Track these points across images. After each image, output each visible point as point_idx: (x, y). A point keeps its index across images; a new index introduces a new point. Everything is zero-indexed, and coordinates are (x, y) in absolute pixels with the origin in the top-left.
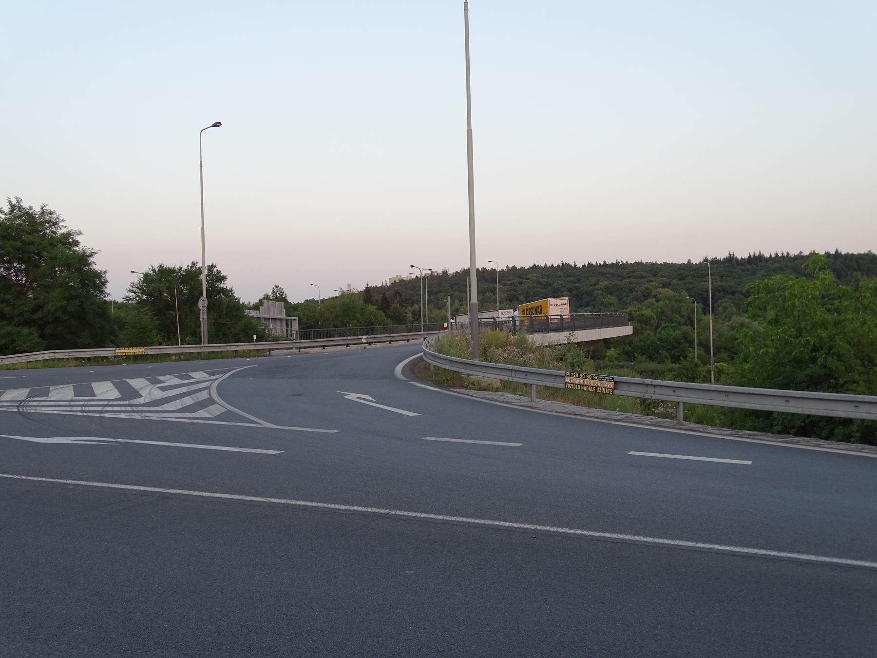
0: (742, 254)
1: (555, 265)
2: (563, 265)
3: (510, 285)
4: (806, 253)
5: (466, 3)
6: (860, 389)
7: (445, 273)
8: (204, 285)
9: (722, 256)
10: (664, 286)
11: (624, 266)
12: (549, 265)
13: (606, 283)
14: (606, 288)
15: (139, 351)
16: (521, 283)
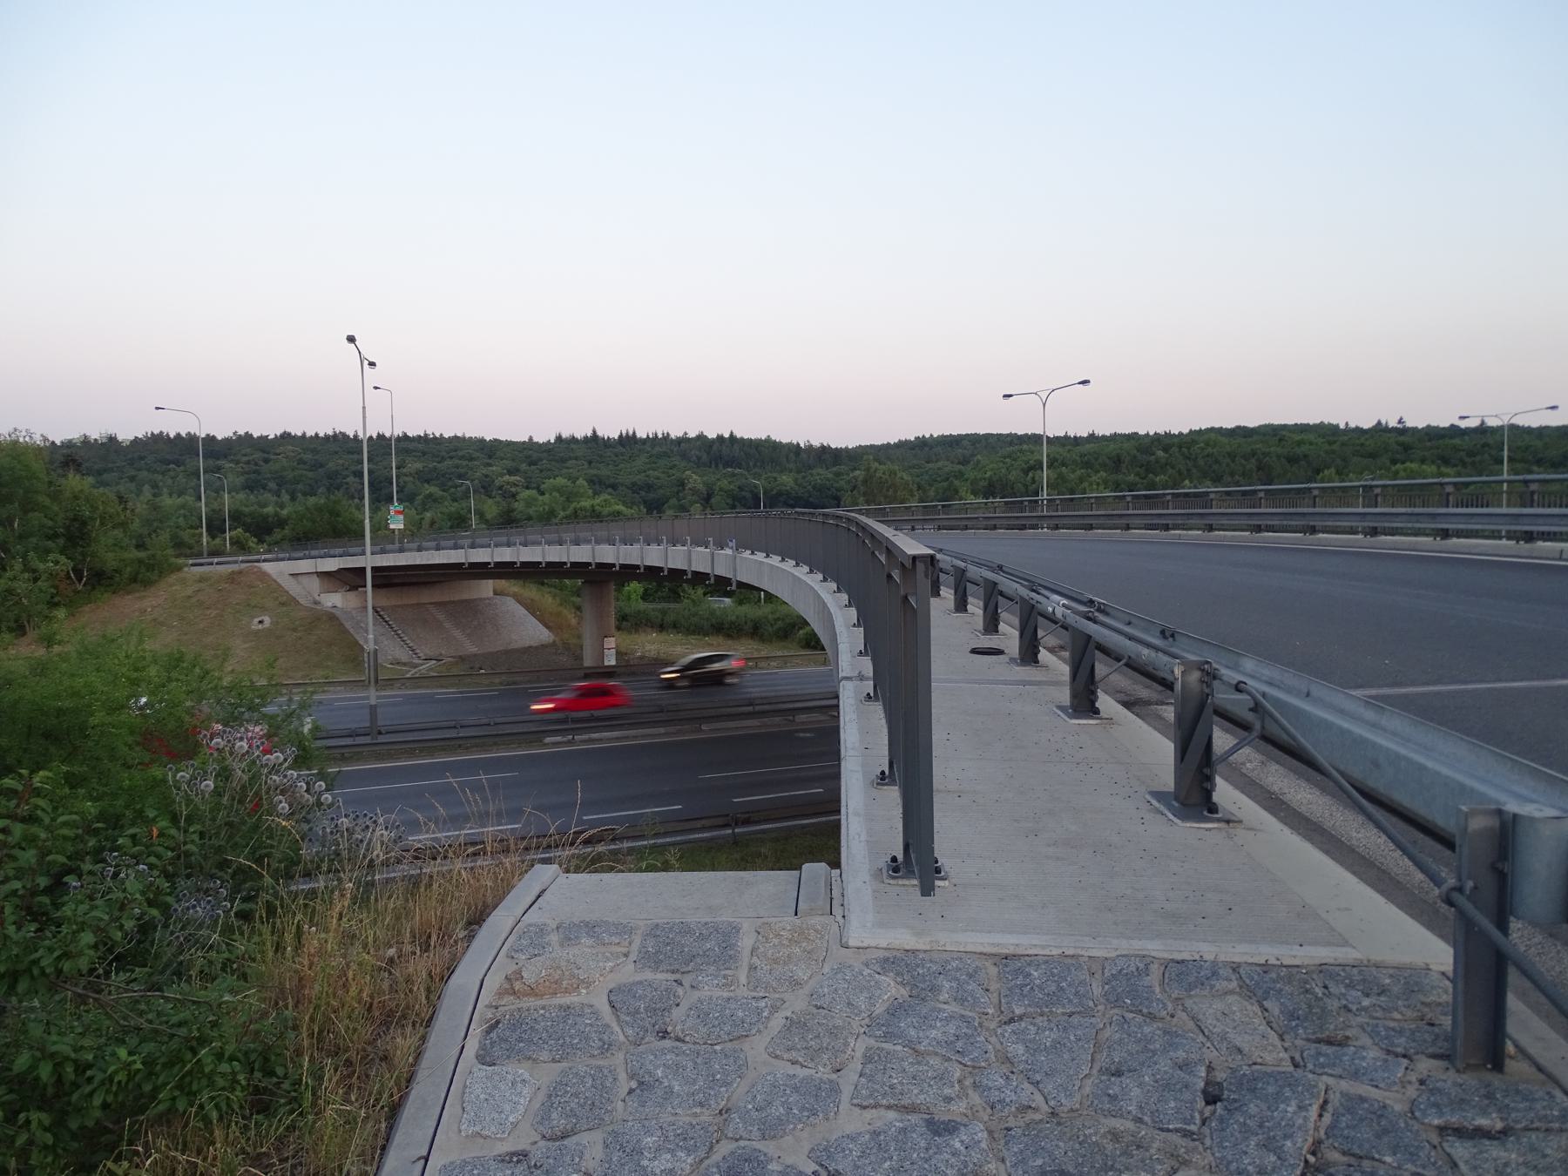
0: (610, 431)
1: (321, 435)
2: (335, 435)
3: (248, 462)
4: (692, 435)
5: (974, 651)
6: (402, 1057)
7: (112, 439)
8: (886, 531)
9: (582, 431)
10: (510, 473)
11: (438, 441)
12: (310, 433)
13: (419, 465)
14: (418, 472)
15: (1292, 510)
16: (266, 461)
